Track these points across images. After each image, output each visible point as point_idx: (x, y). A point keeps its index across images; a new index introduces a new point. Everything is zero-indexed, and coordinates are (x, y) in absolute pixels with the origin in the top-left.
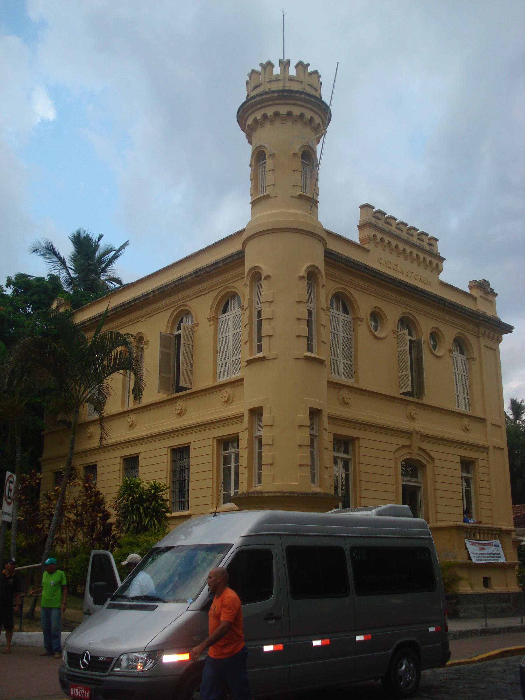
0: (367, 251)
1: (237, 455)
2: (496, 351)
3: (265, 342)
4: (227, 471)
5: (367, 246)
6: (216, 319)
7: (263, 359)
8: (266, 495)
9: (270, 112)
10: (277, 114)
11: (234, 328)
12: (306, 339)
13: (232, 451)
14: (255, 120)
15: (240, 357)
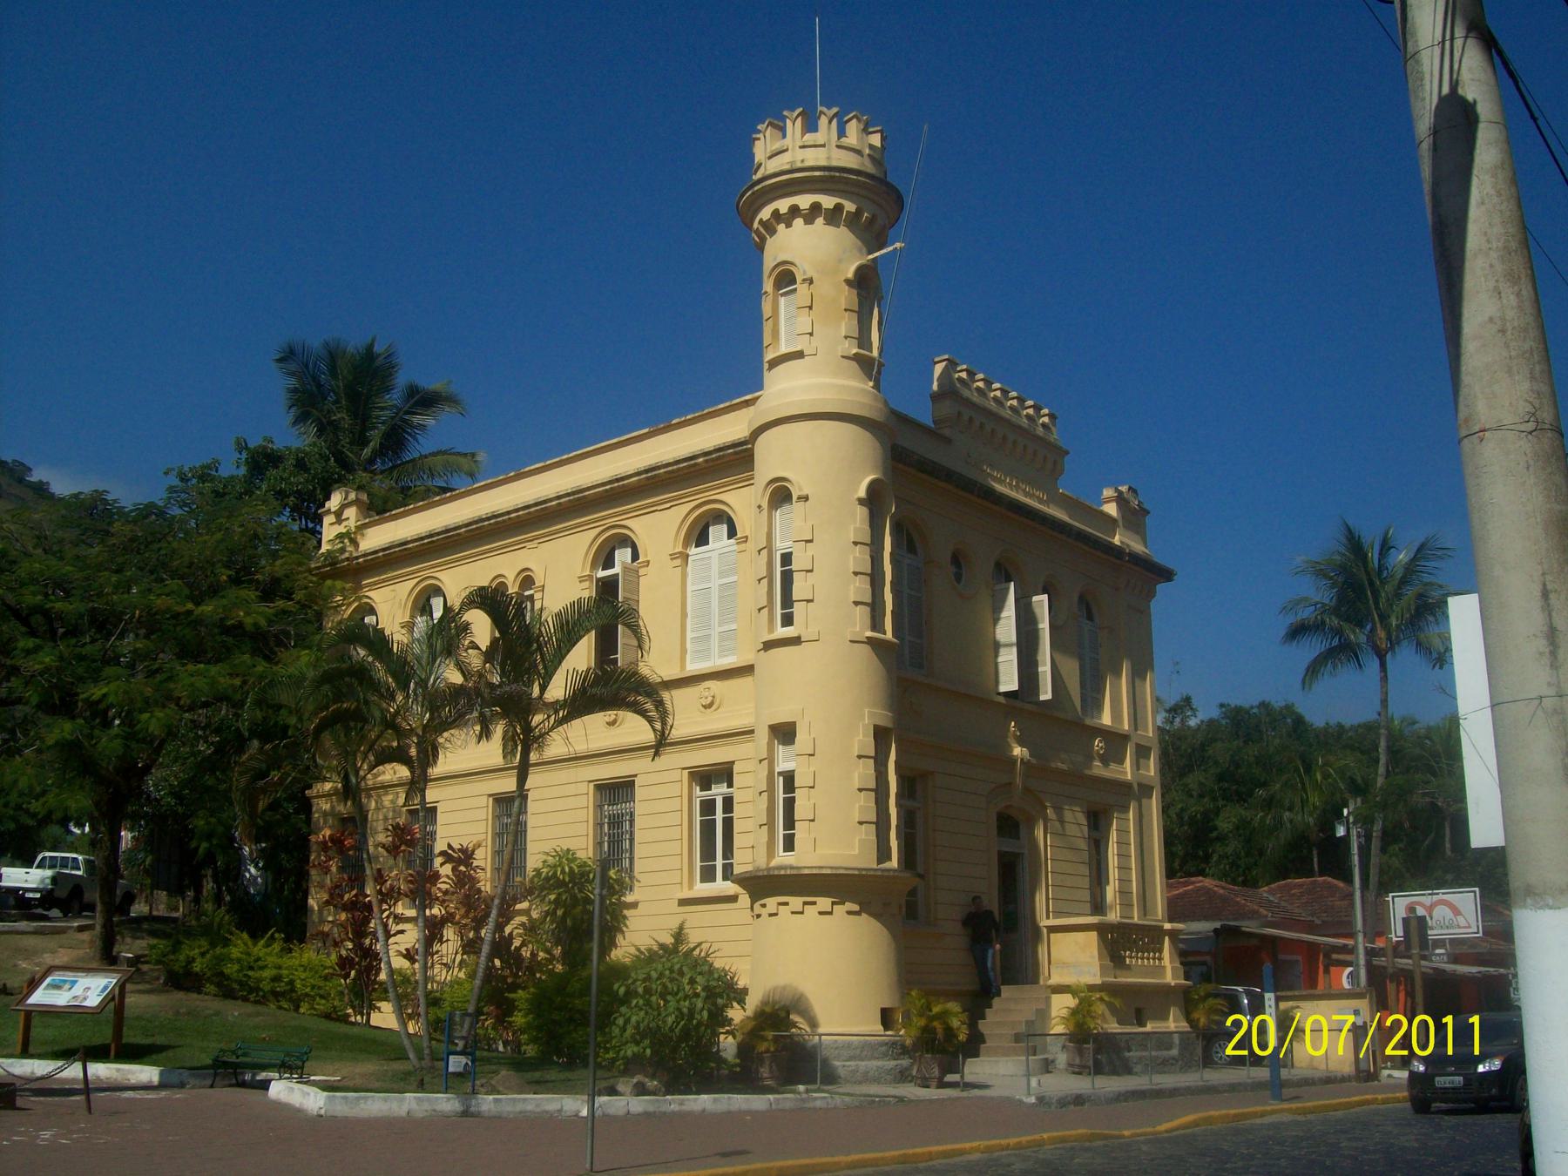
0: (948, 441)
1: (728, 803)
2: (1143, 613)
3: (798, 610)
4: (708, 829)
5: (947, 432)
6: (685, 557)
7: (796, 641)
8: (806, 871)
9: (804, 201)
10: (816, 208)
11: (722, 574)
12: (868, 609)
13: (718, 791)
14: (776, 213)
15: (734, 626)
